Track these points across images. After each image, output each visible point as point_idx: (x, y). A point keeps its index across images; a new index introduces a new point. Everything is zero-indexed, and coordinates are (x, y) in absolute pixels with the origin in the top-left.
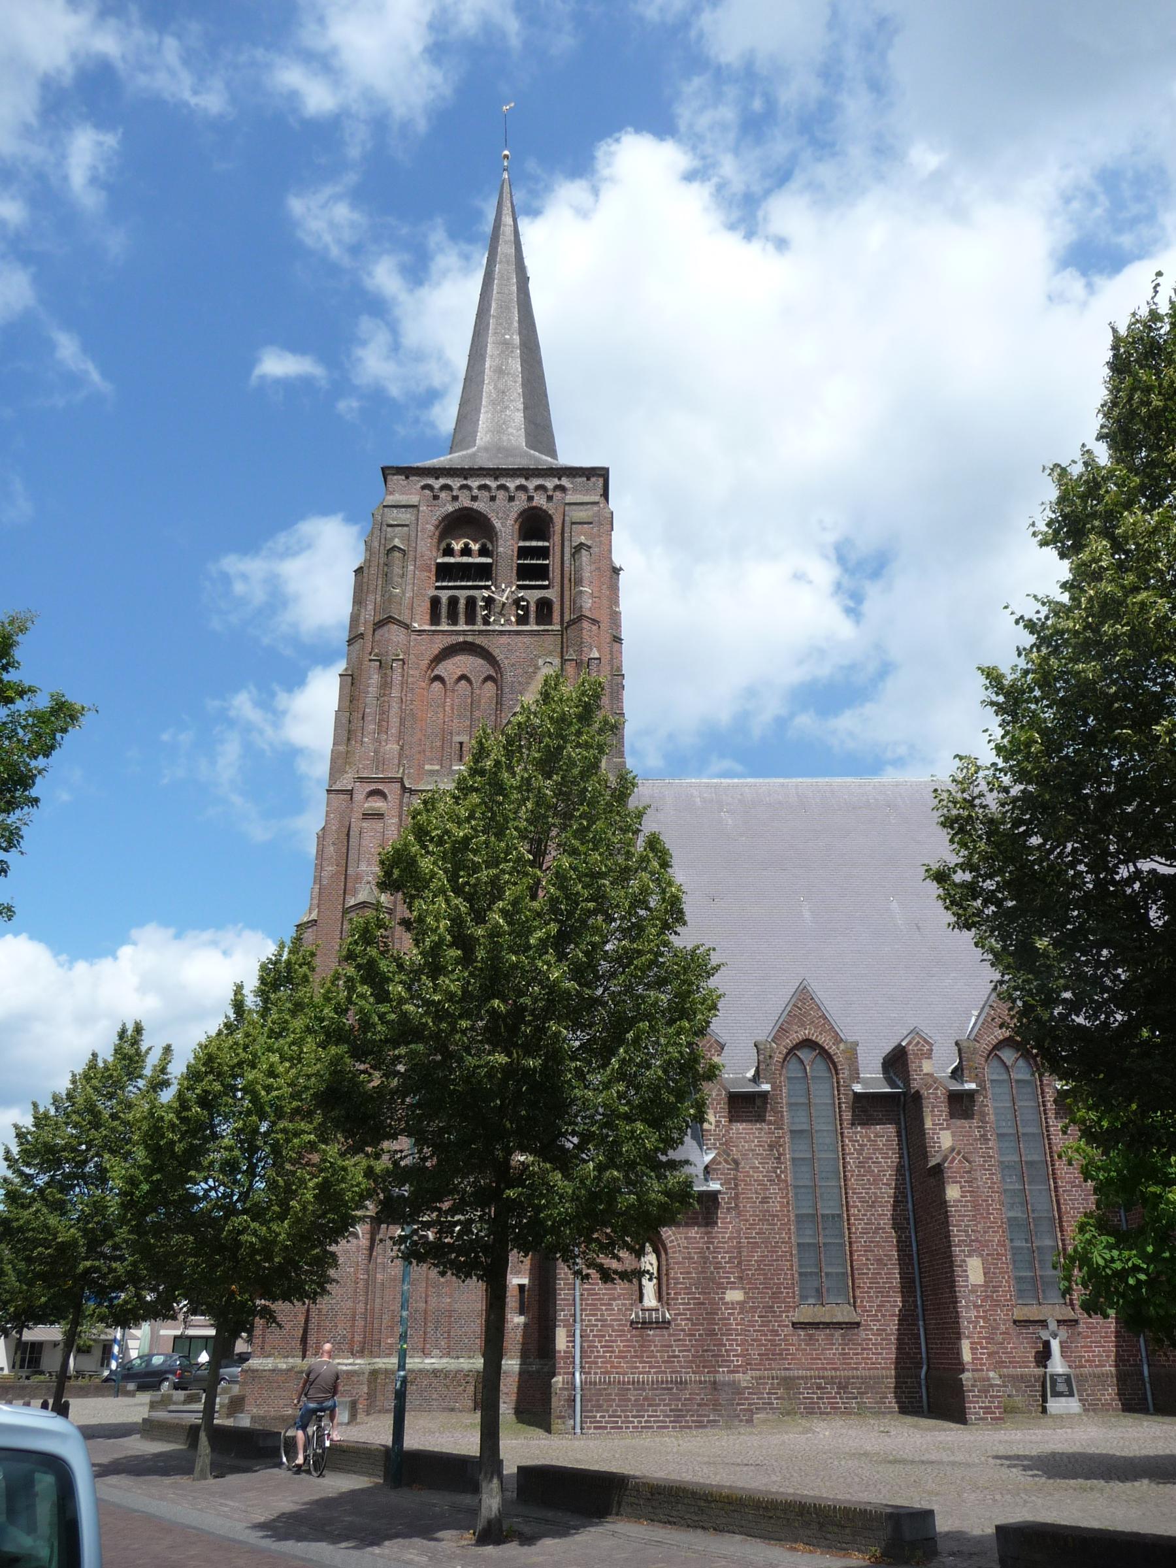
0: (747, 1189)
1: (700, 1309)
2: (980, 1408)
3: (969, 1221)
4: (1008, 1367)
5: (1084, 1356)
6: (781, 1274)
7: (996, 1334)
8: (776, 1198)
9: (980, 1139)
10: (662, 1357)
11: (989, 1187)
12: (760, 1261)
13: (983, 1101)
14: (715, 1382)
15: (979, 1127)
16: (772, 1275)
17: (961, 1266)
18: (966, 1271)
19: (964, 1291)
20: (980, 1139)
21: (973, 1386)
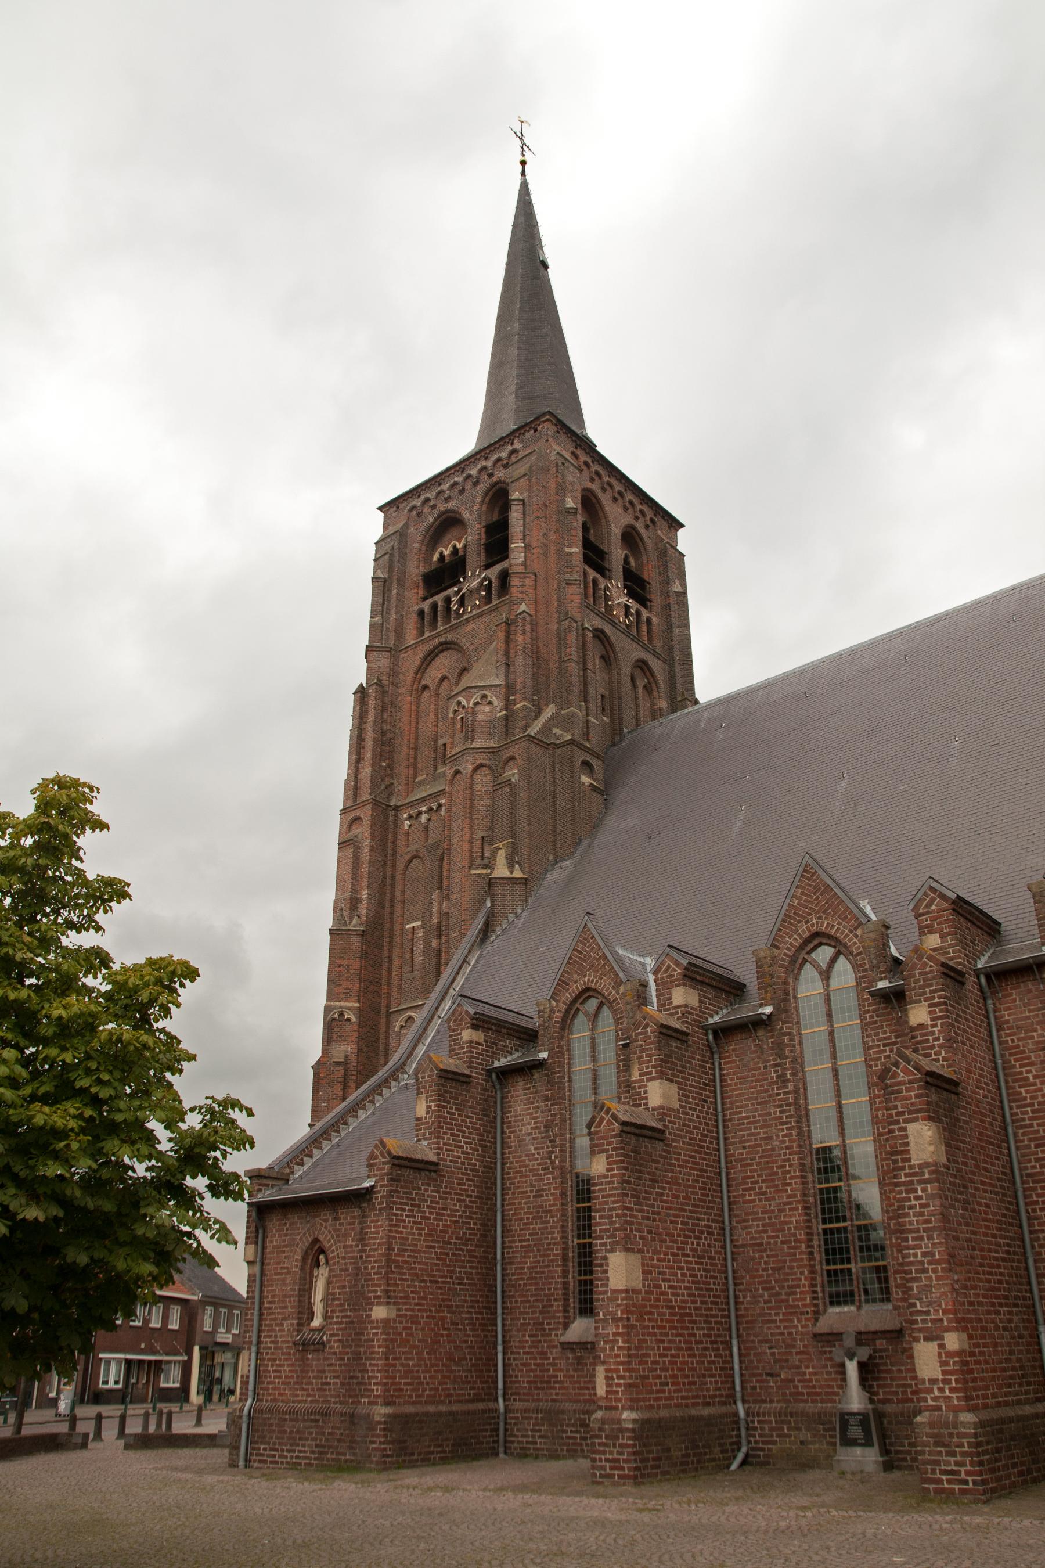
0: (523, 1182)
1: (350, 1328)
2: (607, 1460)
3: (614, 1202)
4: (806, 1401)
5: (910, 1386)
6: (551, 1283)
7: (791, 1353)
8: (549, 1190)
9: (776, 1083)
10: (317, 1384)
11: (787, 1148)
12: (532, 1268)
13: (782, 1028)
14: (352, 1415)
15: (776, 1065)
16: (543, 1284)
17: (601, 1265)
18: (606, 1272)
19: (603, 1300)
20: (776, 1083)
21: (600, 1429)
